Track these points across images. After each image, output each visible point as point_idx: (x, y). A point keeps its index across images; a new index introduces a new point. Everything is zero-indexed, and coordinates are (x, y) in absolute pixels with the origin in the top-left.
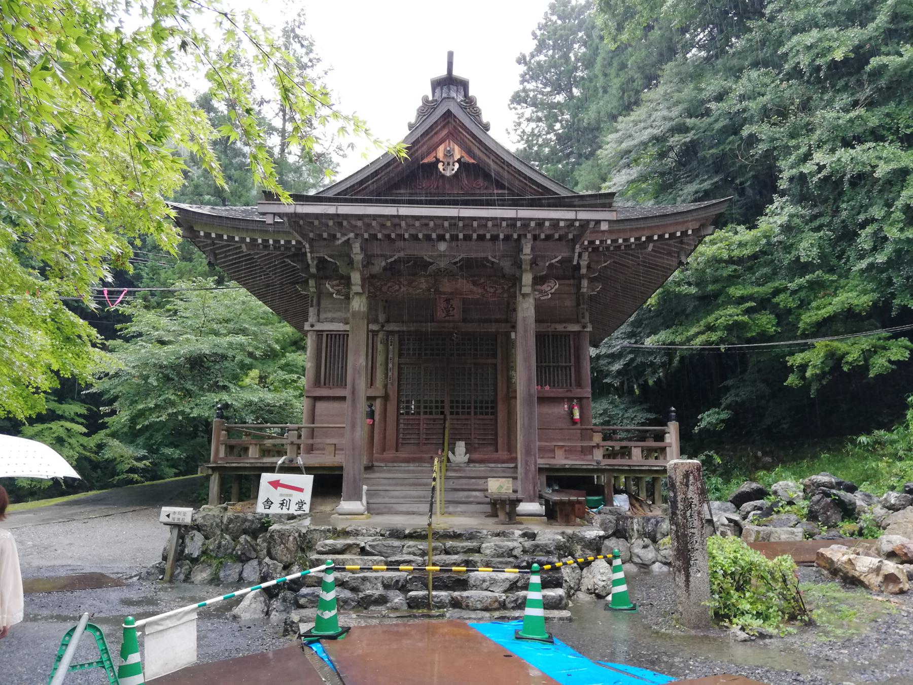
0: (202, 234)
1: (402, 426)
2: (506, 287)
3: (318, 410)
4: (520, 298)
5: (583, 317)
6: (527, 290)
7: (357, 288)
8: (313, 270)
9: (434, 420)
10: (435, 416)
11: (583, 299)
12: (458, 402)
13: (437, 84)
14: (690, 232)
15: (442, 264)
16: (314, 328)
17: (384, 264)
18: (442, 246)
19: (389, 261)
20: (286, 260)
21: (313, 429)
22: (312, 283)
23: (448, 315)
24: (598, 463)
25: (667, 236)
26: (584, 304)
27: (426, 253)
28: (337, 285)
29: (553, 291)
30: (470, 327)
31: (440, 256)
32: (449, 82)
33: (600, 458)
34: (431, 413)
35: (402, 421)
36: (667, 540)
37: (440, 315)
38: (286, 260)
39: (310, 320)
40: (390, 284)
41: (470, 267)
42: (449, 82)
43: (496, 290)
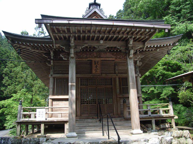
0: (16, 42)
1: (82, 108)
2: (123, 56)
3: (53, 103)
4: (128, 59)
5: (138, 72)
6: (131, 56)
7: (72, 55)
8: (52, 58)
9: (93, 105)
10: (93, 104)
11: (137, 67)
12: (100, 99)
13: (91, 5)
14: (171, 44)
15: (101, 48)
16: (52, 76)
17: (80, 48)
18: (102, 42)
19: (83, 47)
20: (43, 55)
21: (52, 108)
22: (52, 61)
23: (96, 72)
24: (150, 115)
25: (165, 45)
26: (138, 68)
27: (94, 44)
28: (64, 55)
29: (138, 57)
30: (104, 75)
31: (101, 45)
32: (95, 4)
33: (150, 114)
34: (92, 103)
35: (82, 106)
36: (106, 136)
37: (94, 72)
38: (43, 55)
39: (51, 73)
40: (83, 54)
41: (112, 50)
42: (95, 4)
43: (120, 57)
